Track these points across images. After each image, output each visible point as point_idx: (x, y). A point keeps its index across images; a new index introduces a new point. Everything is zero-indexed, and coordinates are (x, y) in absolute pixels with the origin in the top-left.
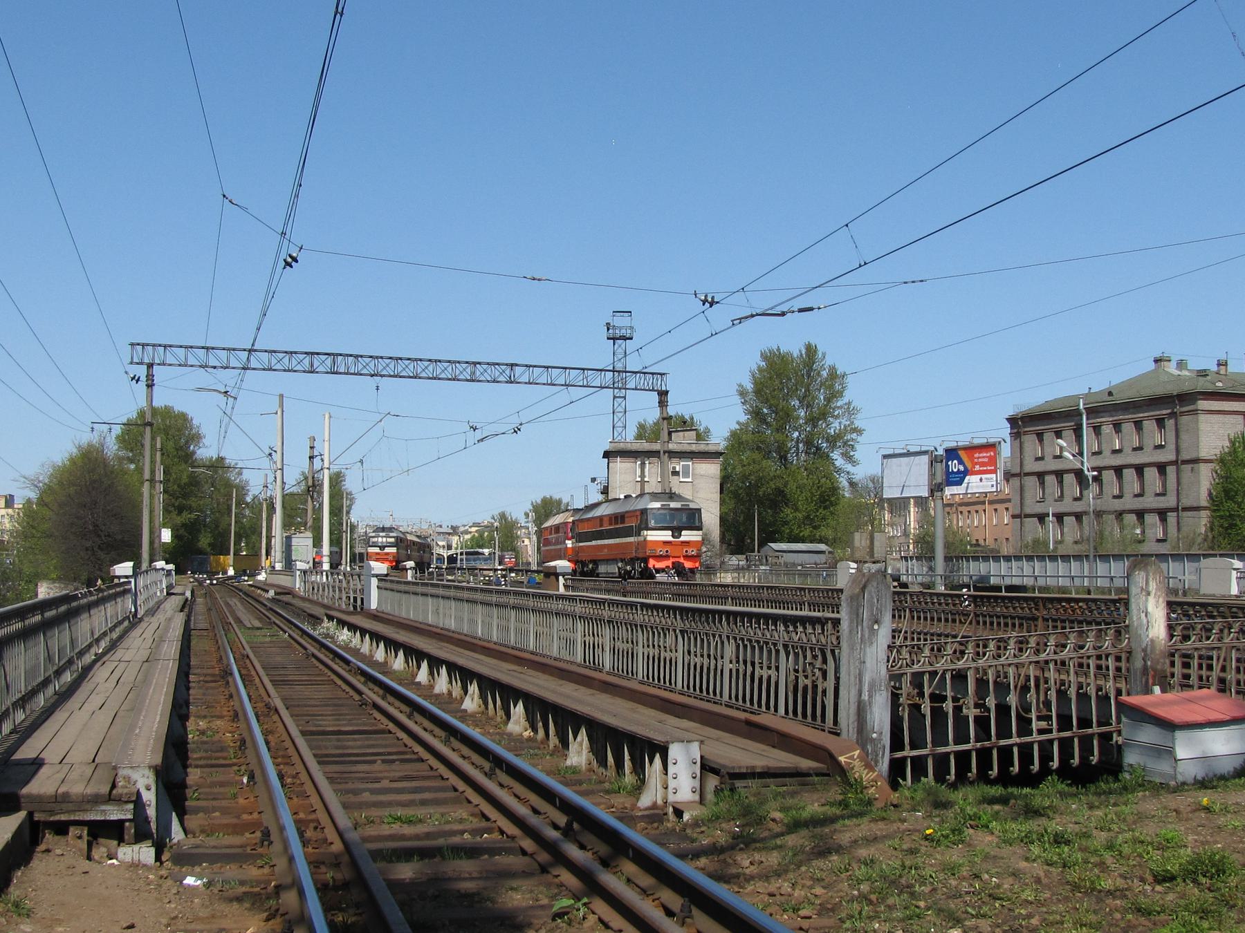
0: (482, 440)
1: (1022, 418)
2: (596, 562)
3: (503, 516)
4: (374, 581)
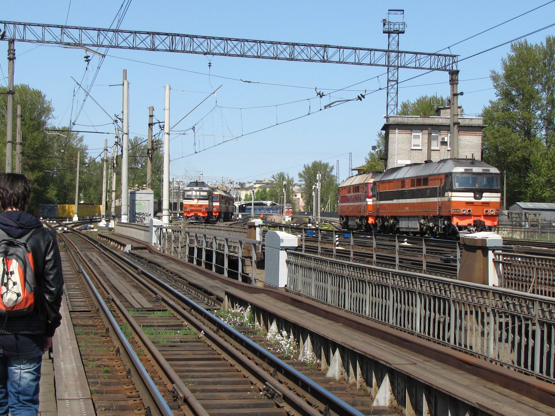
0: (329, 105)
2: (396, 218)
3: (281, 177)
4: (283, 256)
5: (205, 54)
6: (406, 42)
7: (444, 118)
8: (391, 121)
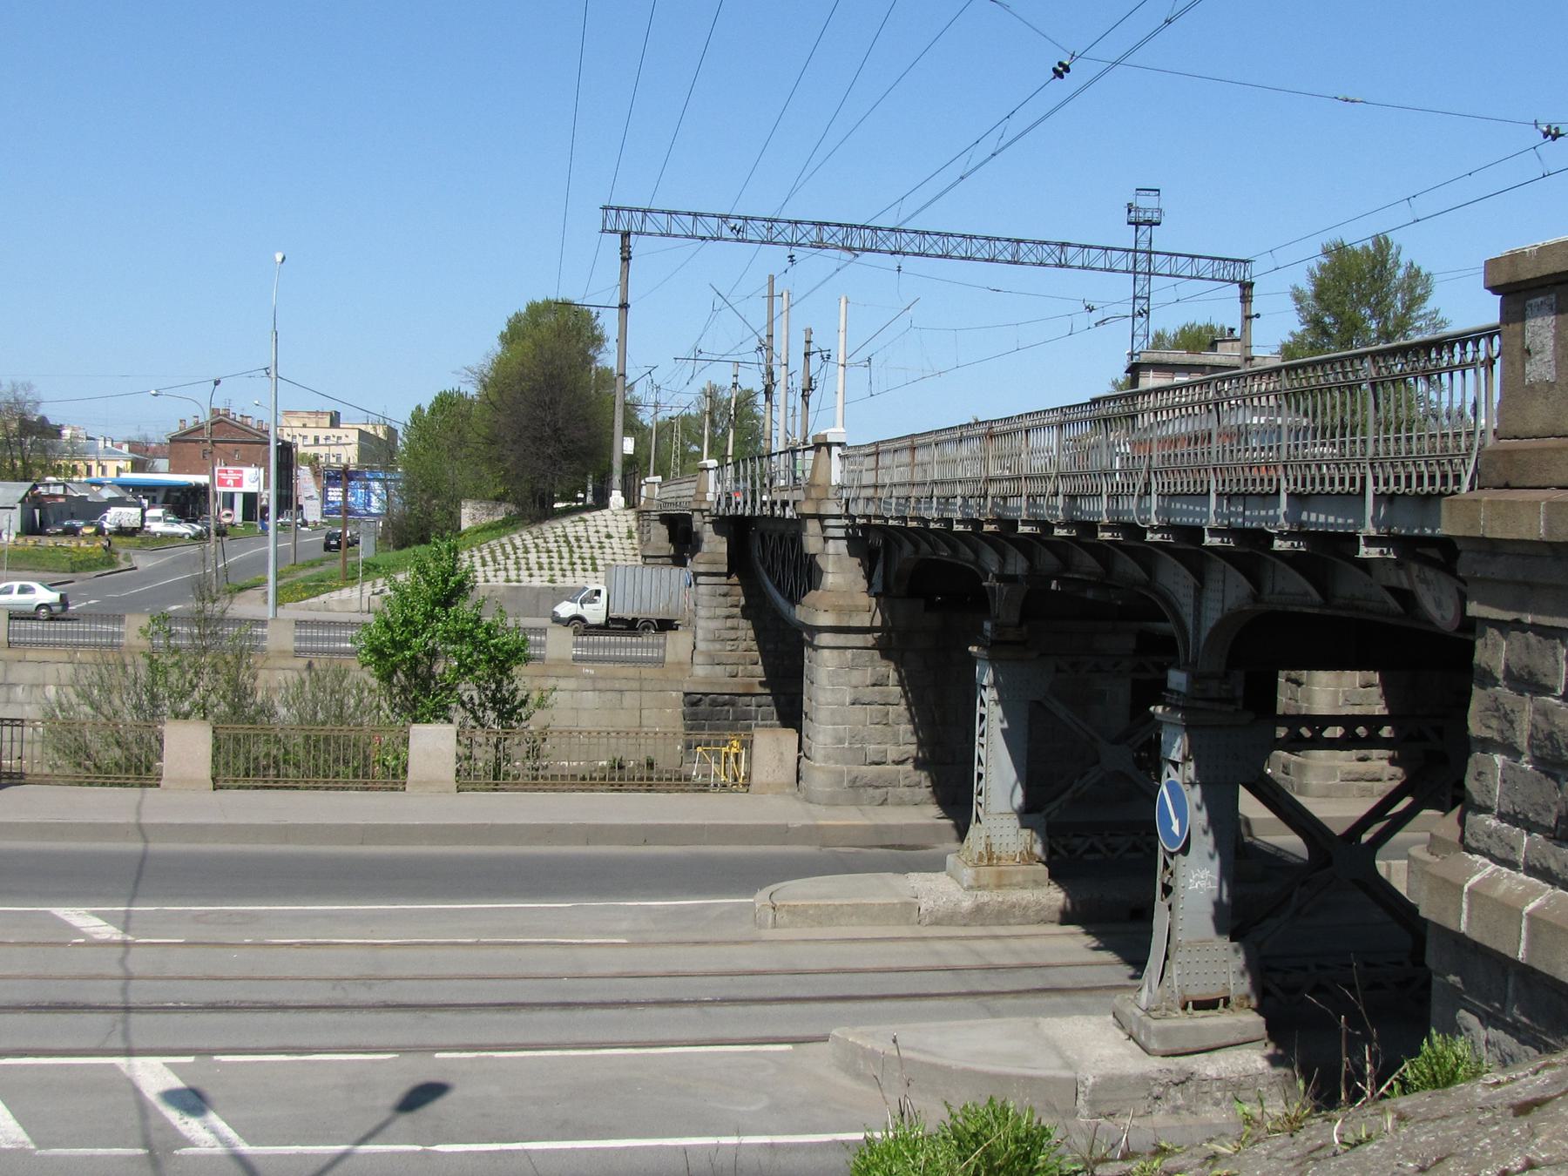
5: (893, 253)
6: (1161, 239)
7: (1226, 354)
8: (1143, 358)
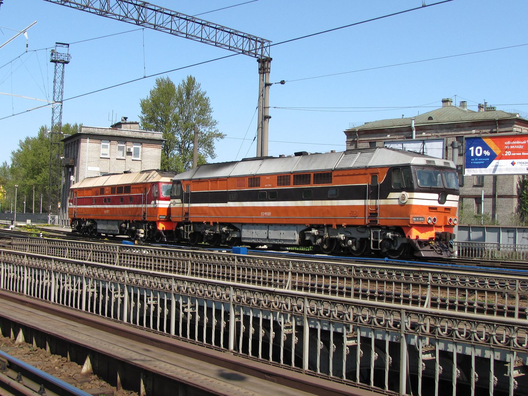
1: (499, 121)
